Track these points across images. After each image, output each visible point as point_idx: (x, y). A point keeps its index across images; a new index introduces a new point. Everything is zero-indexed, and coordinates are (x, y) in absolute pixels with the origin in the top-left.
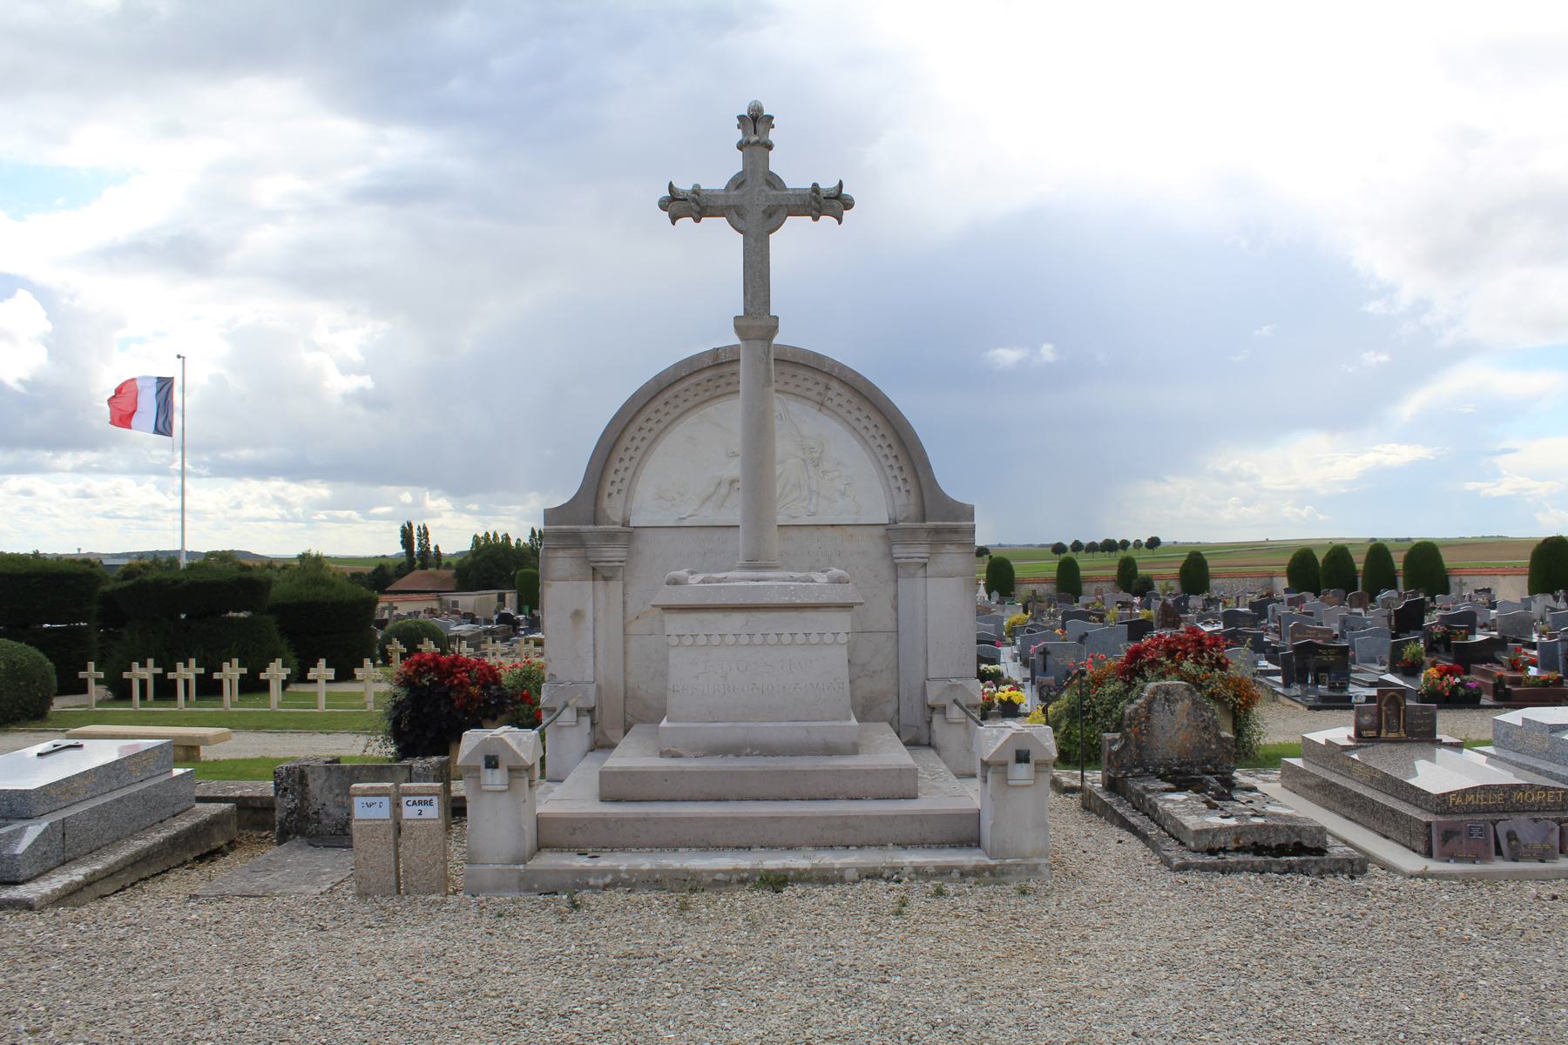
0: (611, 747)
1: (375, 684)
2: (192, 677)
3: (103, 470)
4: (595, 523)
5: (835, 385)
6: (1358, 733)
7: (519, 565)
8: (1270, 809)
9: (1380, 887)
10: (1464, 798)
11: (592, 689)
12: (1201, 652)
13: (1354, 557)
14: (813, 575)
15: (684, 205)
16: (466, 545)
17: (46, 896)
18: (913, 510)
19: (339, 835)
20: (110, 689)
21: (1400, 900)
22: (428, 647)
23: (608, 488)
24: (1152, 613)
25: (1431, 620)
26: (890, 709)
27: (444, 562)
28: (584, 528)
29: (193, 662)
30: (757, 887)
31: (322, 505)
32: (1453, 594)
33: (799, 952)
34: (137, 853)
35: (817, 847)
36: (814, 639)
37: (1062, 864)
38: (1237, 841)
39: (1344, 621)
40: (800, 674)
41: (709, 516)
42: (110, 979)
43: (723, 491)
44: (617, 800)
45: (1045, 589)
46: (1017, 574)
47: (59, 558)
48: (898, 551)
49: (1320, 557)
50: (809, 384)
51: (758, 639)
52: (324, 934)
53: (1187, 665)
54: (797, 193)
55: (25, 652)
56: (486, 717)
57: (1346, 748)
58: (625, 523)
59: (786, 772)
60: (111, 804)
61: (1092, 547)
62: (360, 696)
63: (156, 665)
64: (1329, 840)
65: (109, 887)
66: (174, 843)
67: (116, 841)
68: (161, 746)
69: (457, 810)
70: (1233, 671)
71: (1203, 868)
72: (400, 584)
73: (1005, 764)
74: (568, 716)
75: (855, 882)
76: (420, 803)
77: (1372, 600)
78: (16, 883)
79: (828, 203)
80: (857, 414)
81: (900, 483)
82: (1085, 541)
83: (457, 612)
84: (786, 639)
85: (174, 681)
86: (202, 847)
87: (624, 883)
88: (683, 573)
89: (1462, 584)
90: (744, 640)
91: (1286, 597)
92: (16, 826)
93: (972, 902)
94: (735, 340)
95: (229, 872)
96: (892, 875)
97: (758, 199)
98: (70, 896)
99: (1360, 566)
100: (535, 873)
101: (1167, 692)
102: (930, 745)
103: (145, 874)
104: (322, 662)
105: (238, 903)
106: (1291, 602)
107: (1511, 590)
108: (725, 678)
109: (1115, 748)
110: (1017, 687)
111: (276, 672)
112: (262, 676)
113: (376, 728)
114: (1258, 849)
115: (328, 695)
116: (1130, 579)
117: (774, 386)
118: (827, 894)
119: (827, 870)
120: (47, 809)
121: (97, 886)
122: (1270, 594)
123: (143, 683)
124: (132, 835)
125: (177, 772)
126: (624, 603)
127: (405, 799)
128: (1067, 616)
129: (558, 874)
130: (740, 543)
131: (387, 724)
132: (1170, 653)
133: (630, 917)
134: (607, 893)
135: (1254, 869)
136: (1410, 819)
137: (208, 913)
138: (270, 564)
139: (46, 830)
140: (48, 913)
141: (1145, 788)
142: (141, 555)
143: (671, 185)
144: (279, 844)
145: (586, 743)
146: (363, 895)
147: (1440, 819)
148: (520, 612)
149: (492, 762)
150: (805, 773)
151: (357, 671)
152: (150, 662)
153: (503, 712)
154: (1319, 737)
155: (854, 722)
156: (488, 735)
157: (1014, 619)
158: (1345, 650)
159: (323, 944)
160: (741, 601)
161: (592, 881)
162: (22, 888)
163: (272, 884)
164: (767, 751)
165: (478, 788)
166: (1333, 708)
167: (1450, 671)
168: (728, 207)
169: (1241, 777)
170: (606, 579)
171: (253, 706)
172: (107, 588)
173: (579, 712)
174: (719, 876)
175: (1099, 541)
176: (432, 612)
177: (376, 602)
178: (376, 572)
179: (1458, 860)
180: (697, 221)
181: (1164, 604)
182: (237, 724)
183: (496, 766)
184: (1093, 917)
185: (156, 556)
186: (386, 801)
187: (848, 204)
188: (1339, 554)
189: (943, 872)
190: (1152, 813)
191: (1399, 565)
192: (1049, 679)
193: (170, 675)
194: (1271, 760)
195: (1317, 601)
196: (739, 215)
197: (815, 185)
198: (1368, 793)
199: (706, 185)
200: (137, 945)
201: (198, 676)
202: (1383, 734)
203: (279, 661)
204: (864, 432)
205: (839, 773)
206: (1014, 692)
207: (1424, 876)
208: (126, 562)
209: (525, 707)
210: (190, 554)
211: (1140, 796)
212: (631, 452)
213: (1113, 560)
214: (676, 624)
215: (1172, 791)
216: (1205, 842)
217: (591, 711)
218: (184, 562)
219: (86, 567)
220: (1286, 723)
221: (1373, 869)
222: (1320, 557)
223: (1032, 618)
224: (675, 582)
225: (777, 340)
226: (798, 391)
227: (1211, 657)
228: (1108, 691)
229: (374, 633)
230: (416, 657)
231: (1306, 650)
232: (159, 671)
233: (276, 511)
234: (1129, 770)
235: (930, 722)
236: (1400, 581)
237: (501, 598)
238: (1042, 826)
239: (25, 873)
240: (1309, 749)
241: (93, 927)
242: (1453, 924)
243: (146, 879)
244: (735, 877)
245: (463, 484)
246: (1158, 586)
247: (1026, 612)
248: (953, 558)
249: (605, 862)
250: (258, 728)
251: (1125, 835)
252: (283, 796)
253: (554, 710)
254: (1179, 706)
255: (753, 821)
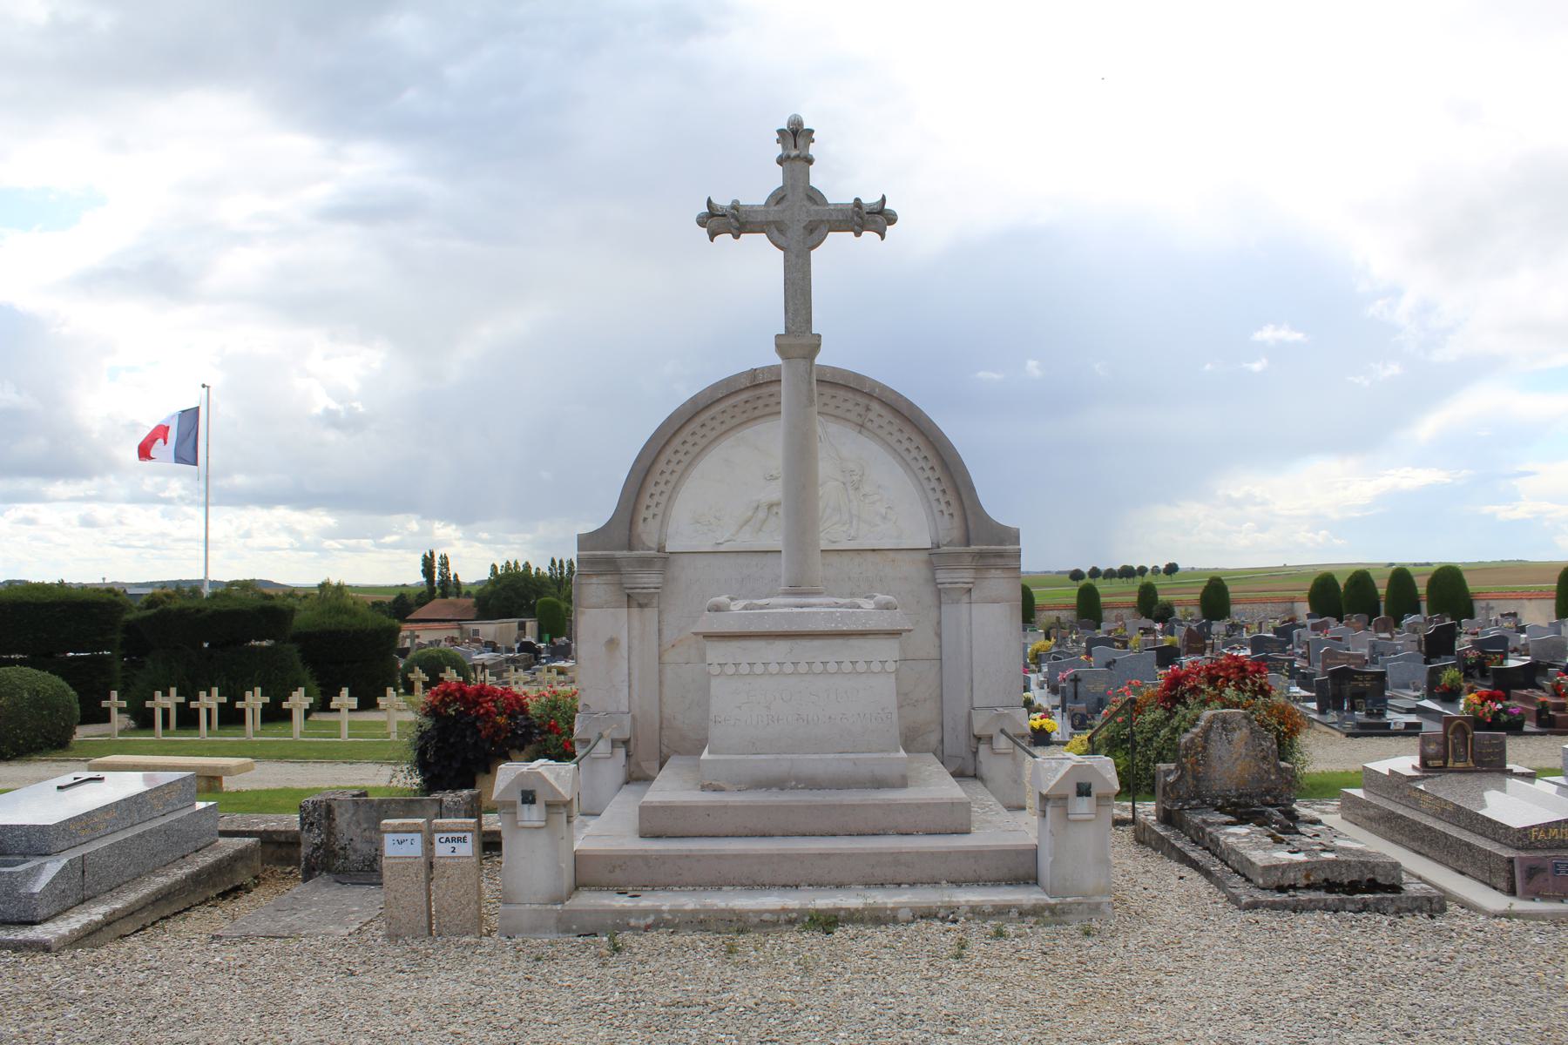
0: (647, 779)
1: (400, 714)
2: (215, 707)
3: (99, 498)
4: (630, 547)
5: (875, 406)
6: (1424, 763)
7: (539, 594)
8: (1339, 843)
9: (1463, 927)
10: (1547, 832)
11: (627, 720)
12: (1244, 678)
13: (1377, 583)
14: (860, 601)
15: (724, 221)
16: (485, 575)
17: (64, 937)
18: (956, 534)
19: (368, 871)
20: (132, 718)
21: (1487, 942)
22: (450, 675)
23: (643, 513)
24: (1176, 639)
25: (1463, 643)
26: (934, 739)
27: (464, 591)
28: (618, 554)
29: (215, 690)
30: (806, 929)
31: (330, 534)
32: (1479, 618)
33: (857, 1000)
34: (159, 890)
35: (868, 885)
36: (861, 667)
37: (1123, 902)
38: (1307, 877)
39: (1373, 646)
40: (848, 701)
41: (747, 540)
42: (129, 1029)
43: (761, 515)
44: (658, 837)
45: (1066, 616)
46: (1231, 596)
47: (83, 587)
48: (942, 576)
49: (1342, 582)
50: (849, 405)
51: (803, 668)
52: (353, 980)
53: (1230, 692)
54: (840, 208)
55: (48, 682)
56: (512, 747)
57: (1412, 779)
58: (661, 549)
59: (834, 806)
60: (132, 839)
61: (1110, 574)
62: (383, 725)
63: (178, 694)
64: (1404, 876)
65: (128, 927)
66: (196, 879)
67: (137, 878)
68: (184, 779)
69: (491, 844)
70: (1277, 698)
71: (1273, 906)
72: (420, 613)
73: (1065, 798)
74: (603, 748)
75: (908, 922)
76: (453, 840)
77: (1398, 625)
78: (33, 923)
79: (871, 218)
80: (898, 435)
81: (943, 507)
82: (1103, 567)
83: (479, 641)
84: (832, 667)
85: (197, 710)
86: (222, 884)
87: (667, 924)
88: (724, 599)
89: (1489, 609)
90: (789, 668)
91: (1309, 622)
92: (34, 862)
93: (1035, 944)
94: (777, 360)
95: (255, 910)
96: (948, 915)
97: (799, 216)
98: (88, 937)
99: (1382, 591)
100: (573, 913)
101: (1224, 721)
102: (975, 776)
103: (167, 912)
104: (345, 691)
105: (262, 944)
106: (1314, 628)
107: (1538, 615)
108: (768, 708)
109: (1171, 779)
110: (1047, 715)
111: (299, 701)
112: (285, 705)
113: (401, 758)
114: (1330, 886)
115: (351, 724)
116: (1150, 605)
117: (816, 409)
118: (881, 935)
119: (880, 909)
120: (66, 844)
121: (117, 925)
122: (1292, 620)
123: (166, 712)
124: (153, 872)
125: (200, 805)
126: (660, 630)
127: (437, 836)
128: (1092, 642)
129: (597, 914)
130: (782, 568)
131: (412, 755)
132: (1212, 680)
133: (675, 961)
134: (649, 935)
135: (1326, 908)
136: (1490, 854)
137: (232, 955)
138: (291, 592)
139: (64, 868)
140: (66, 956)
141: (1204, 821)
142: (164, 585)
143: (709, 201)
144: (305, 880)
145: (620, 775)
146: (393, 937)
147: (1523, 854)
148: (540, 640)
149: (529, 798)
150: (853, 807)
151: (380, 700)
152: (173, 690)
153: (530, 743)
154: (1383, 767)
155: (902, 753)
156: (525, 769)
157: (1037, 646)
158: (1381, 676)
159: (352, 990)
160: (786, 628)
161: (633, 922)
162: (39, 928)
163: (298, 924)
164: (813, 784)
165: (515, 825)
166: (1371, 735)
167: (1491, 697)
168: (768, 223)
169: (1302, 809)
170: (641, 606)
171: (274, 735)
172: (129, 617)
173: (614, 743)
174: (766, 917)
175: (1117, 567)
176: (452, 640)
177: (399, 630)
178: (396, 601)
179: (1545, 898)
180: (736, 237)
181: (1189, 630)
182: (260, 753)
183: (533, 802)
184: (1163, 960)
185: (178, 584)
186: (418, 837)
187: (891, 219)
188: (1361, 580)
189: (1001, 911)
190: (1213, 847)
191: (1422, 589)
192: (1081, 707)
193: (193, 704)
194: (1324, 789)
195: (1341, 626)
196: (781, 231)
197: (857, 200)
198: (1439, 826)
199: (745, 201)
200: (157, 991)
201: (220, 705)
202: (1450, 764)
203: (302, 690)
204: (905, 454)
205: (888, 807)
206: (1046, 720)
207: (1509, 915)
208: (149, 591)
209: (553, 737)
210: (214, 583)
211: (1199, 829)
212: (667, 476)
213: (1136, 584)
214: (717, 653)
215: (1233, 824)
216: (1274, 879)
217: (626, 743)
218: (206, 591)
219: (111, 596)
220: (1325, 751)
221: (1452, 908)
222: (1342, 582)
223: (1056, 644)
224: (717, 609)
225: (821, 359)
226: (838, 412)
227: (1254, 683)
228: (1148, 719)
229: (395, 663)
230: (441, 687)
231: (1341, 676)
232: (182, 700)
233: (285, 540)
234: (1186, 802)
235: (975, 753)
236: (1424, 606)
237: (522, 627)
238: (1105, 862)
239: (42, 912)
240: (1370, 780)
241: (112, 971)
242: (1550, 970)
243: (167, 918)
244: (783, 917)
245: (464, 511)
246: (1179, 612)
247: (1048, 637)
248: (1000, 585)
249: (647, 901)
250: (281, 758)
251: (1186, 871)
252: (309, 831)
253: (588, 741)
254: (1237, 736)
255: (800, 858)
